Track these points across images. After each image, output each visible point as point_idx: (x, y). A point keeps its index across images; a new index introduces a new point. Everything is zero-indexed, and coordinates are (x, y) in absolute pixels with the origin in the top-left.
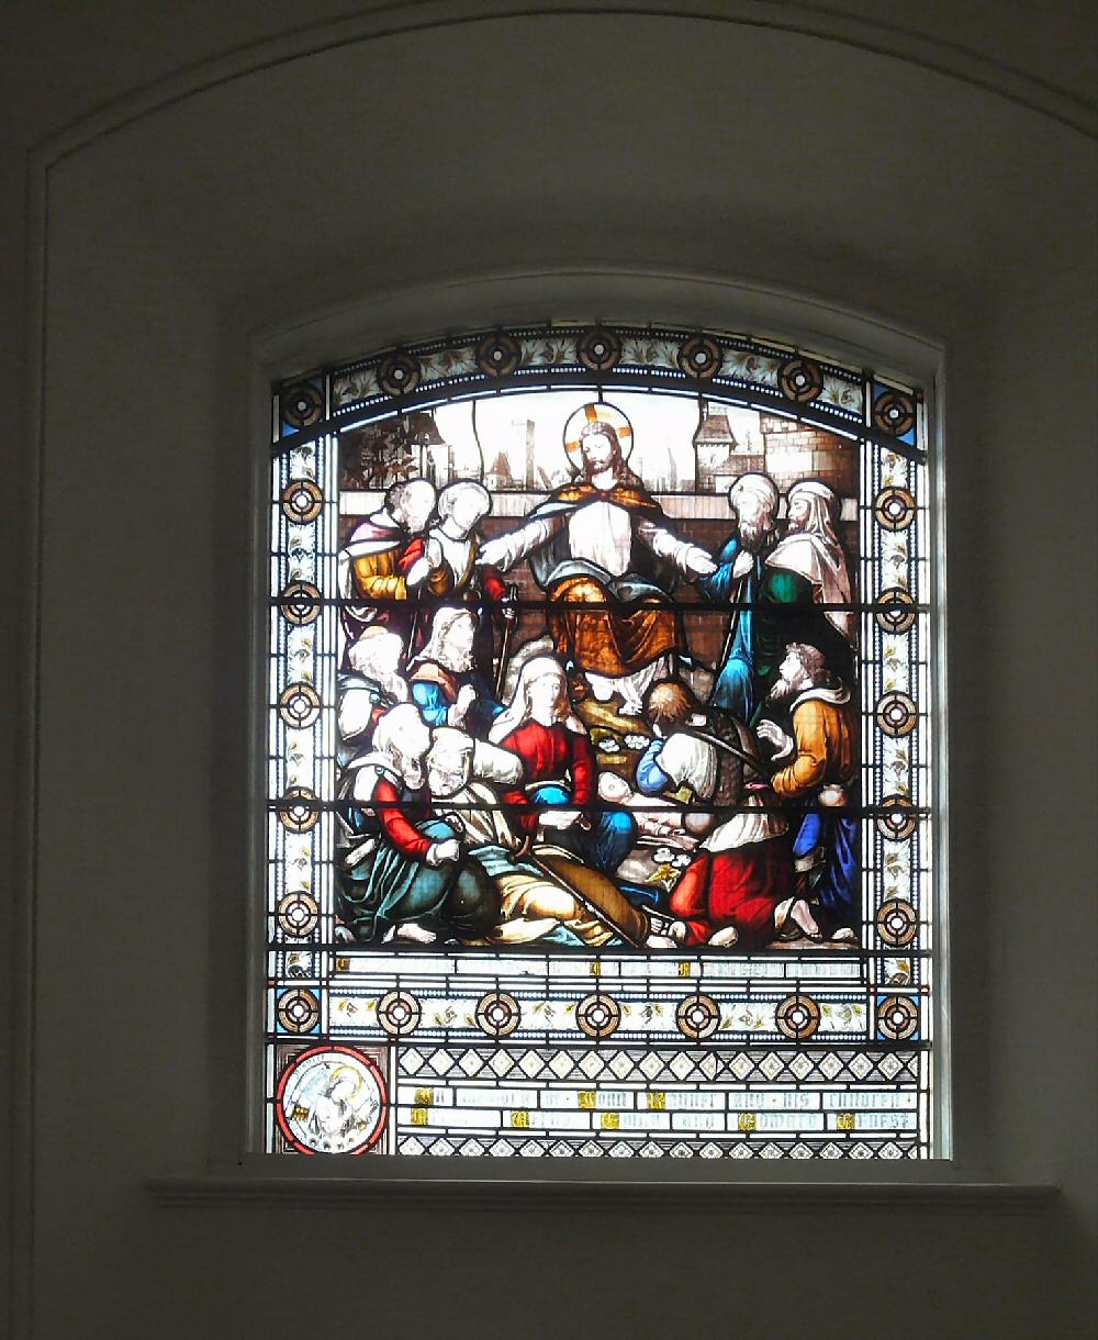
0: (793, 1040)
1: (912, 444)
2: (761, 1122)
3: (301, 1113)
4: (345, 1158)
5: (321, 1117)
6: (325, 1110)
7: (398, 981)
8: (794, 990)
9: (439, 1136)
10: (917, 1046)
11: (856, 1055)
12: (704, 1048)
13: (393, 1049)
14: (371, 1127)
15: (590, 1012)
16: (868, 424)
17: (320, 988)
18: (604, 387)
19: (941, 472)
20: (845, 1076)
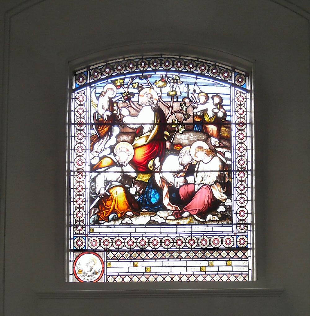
0: (178, 249)
1: (245, 88)
2: (174, 269)
3: (80, 272)
4: (92, 283)
7: (130, 234)
8: (191, 235)
9: (240, 274)
11: (231, 251)
12: (156, 251)
13: (105, 252)
14: (99, 274)
15: (128, 242)
16: (233, 82)
17: (236, 233)
19: (253, 95)
20: (204, 257)
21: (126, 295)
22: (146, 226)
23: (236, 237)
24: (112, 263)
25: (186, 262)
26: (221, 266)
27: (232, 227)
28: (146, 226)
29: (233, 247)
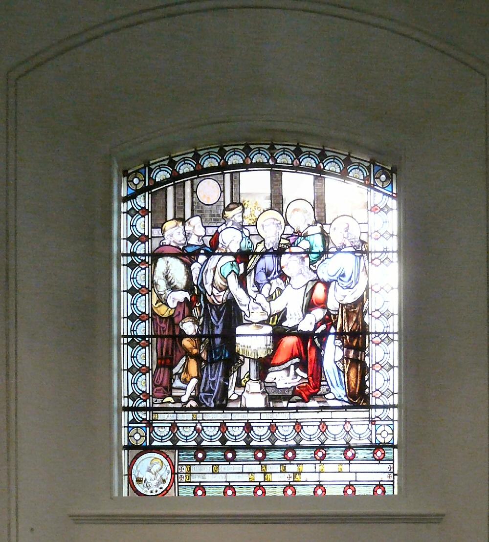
2: (360, 477)
3: (139, 480)
5: (148, 480)
6: (147, 476)
10: (129, 447)
18: (225, 172)
21: (176, 518)
22: (248, 411)
23: (128, 430)
24: (192, 466)
25: (279, 466)
26: (383, 472)
27: (369, 411)
28: (248, 411)
29: (144, 444)
